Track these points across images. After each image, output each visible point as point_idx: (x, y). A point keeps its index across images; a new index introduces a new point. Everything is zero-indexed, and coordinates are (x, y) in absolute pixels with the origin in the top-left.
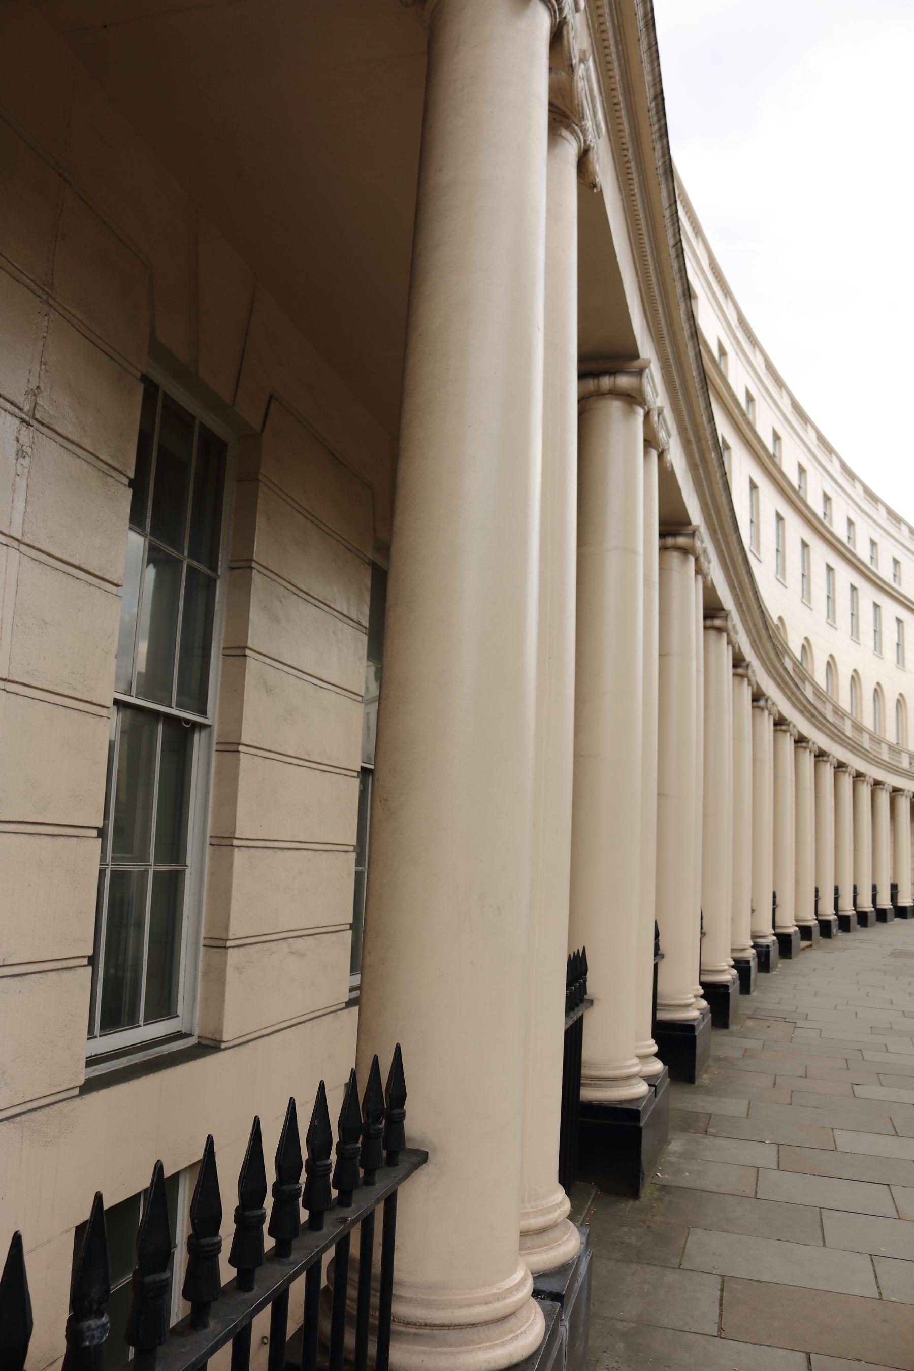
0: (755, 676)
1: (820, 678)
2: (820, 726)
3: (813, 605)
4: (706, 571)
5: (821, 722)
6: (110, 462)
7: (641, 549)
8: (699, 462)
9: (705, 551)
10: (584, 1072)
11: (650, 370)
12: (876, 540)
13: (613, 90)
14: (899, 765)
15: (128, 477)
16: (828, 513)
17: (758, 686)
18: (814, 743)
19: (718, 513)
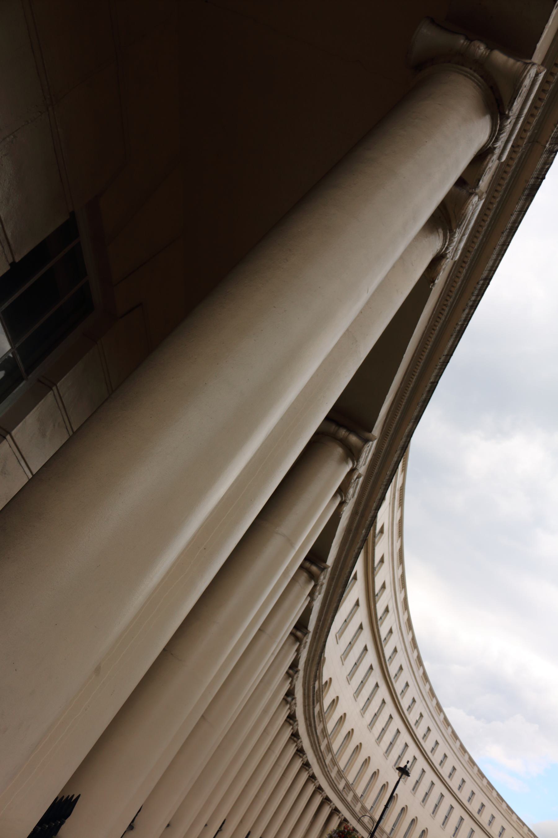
0: (296, 680)
2: (310, 734)
3: (345, 663)
4: (315, 597)
5: (312, 732)
6: (11, 242)
7: (297, 547)
8: (353, 530)
9: (322, 585)
11: (372, 444)
12: (398, 649)
13: (469, 251)
15: (13, 258)
16: (383, 618)
17: (294, 688)
18: (301, 742)
19: (342, 569)
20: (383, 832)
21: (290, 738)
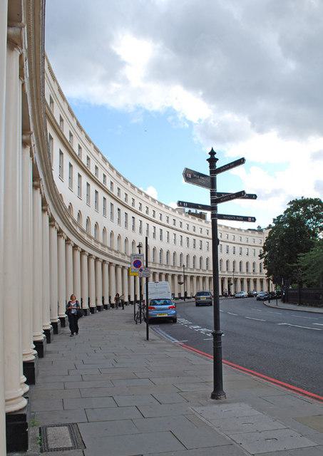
1: (75, 217)
21: (66, 244)
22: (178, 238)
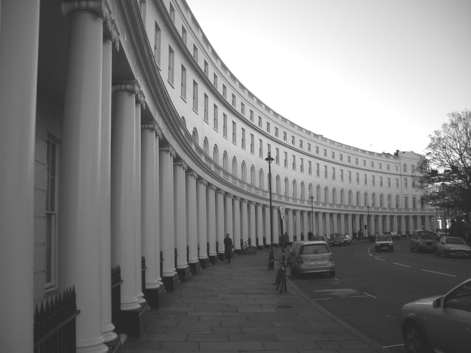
10: (121, 302)
14: (251, 192)
20: (274, 194)
21: (186, 176)
22: (322, 169)
